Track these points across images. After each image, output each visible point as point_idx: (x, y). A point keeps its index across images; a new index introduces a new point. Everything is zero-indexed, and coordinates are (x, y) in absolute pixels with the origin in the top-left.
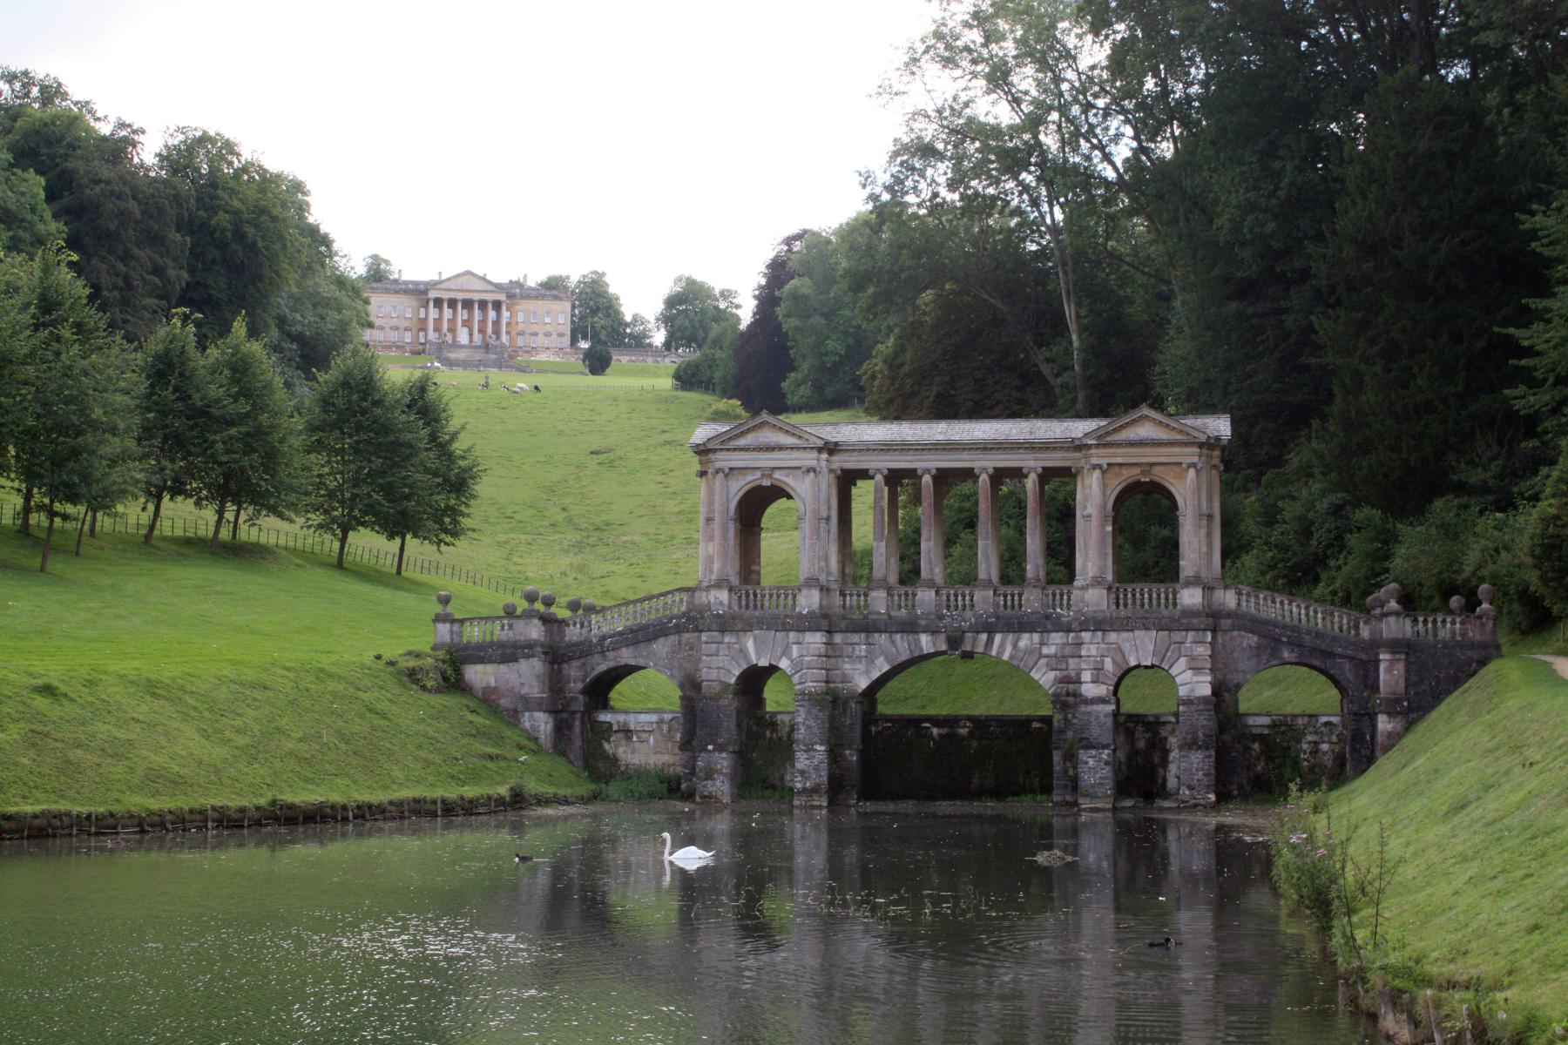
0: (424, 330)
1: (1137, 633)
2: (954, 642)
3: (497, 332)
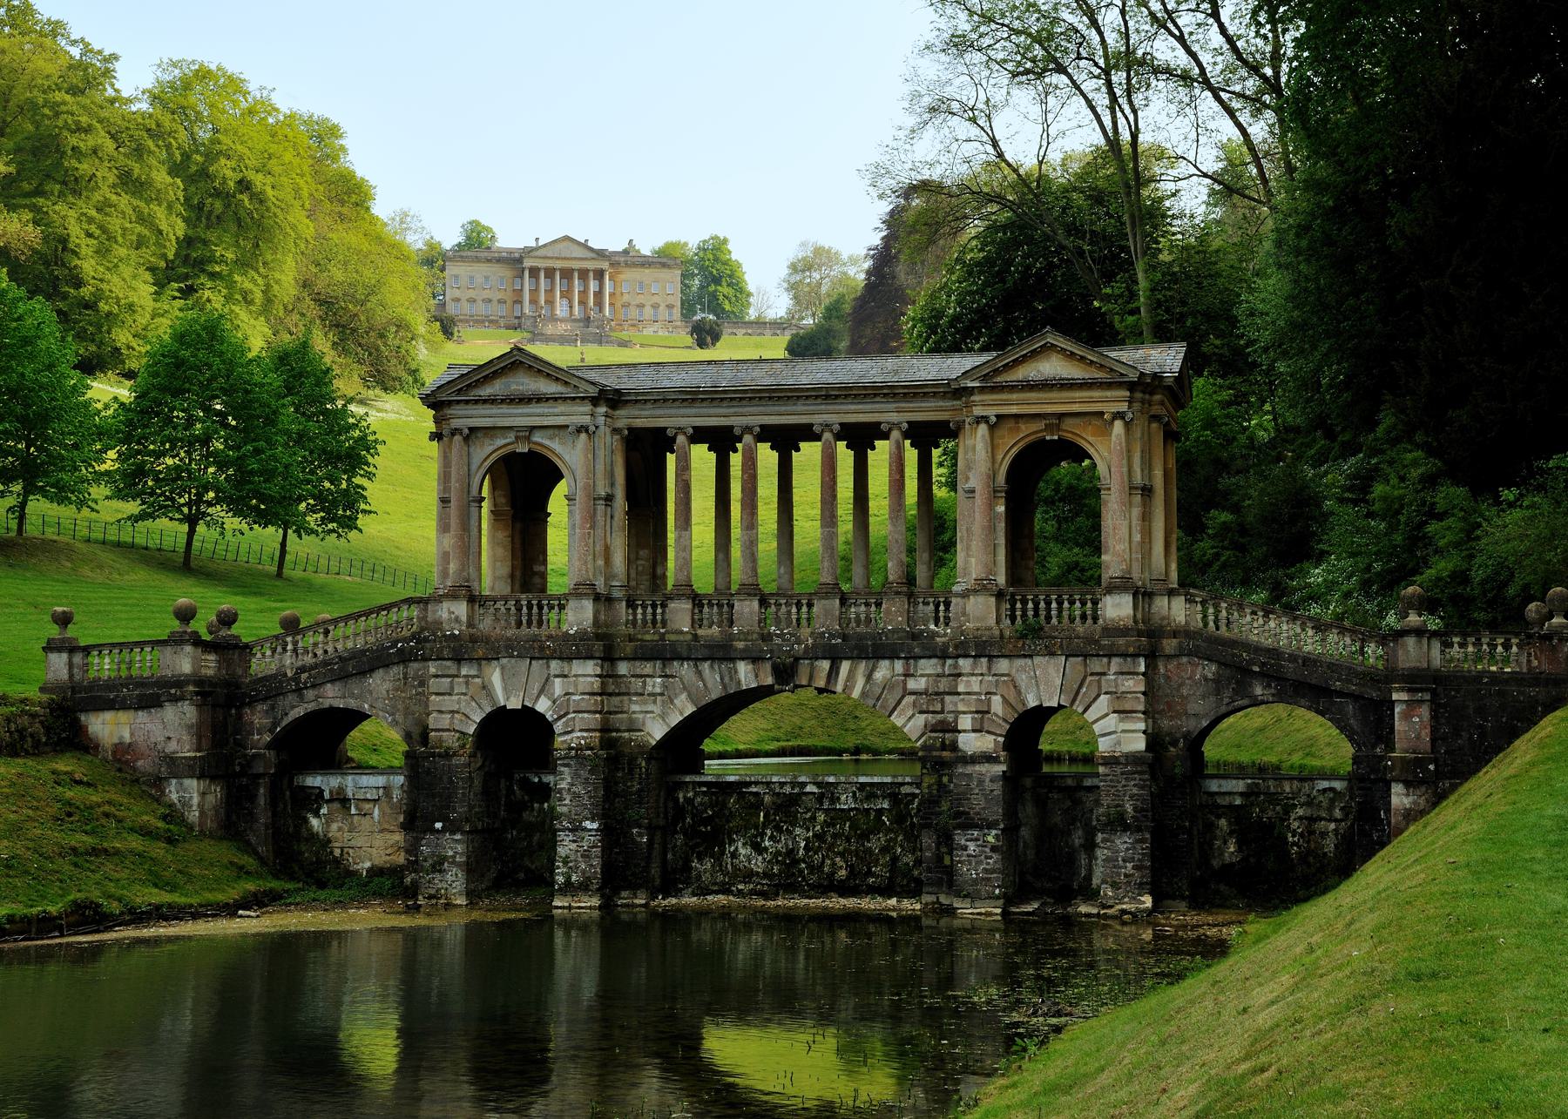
0: (520, 302)
1: (1037, 660)
2: (785, 674)
3: (599, 304)
